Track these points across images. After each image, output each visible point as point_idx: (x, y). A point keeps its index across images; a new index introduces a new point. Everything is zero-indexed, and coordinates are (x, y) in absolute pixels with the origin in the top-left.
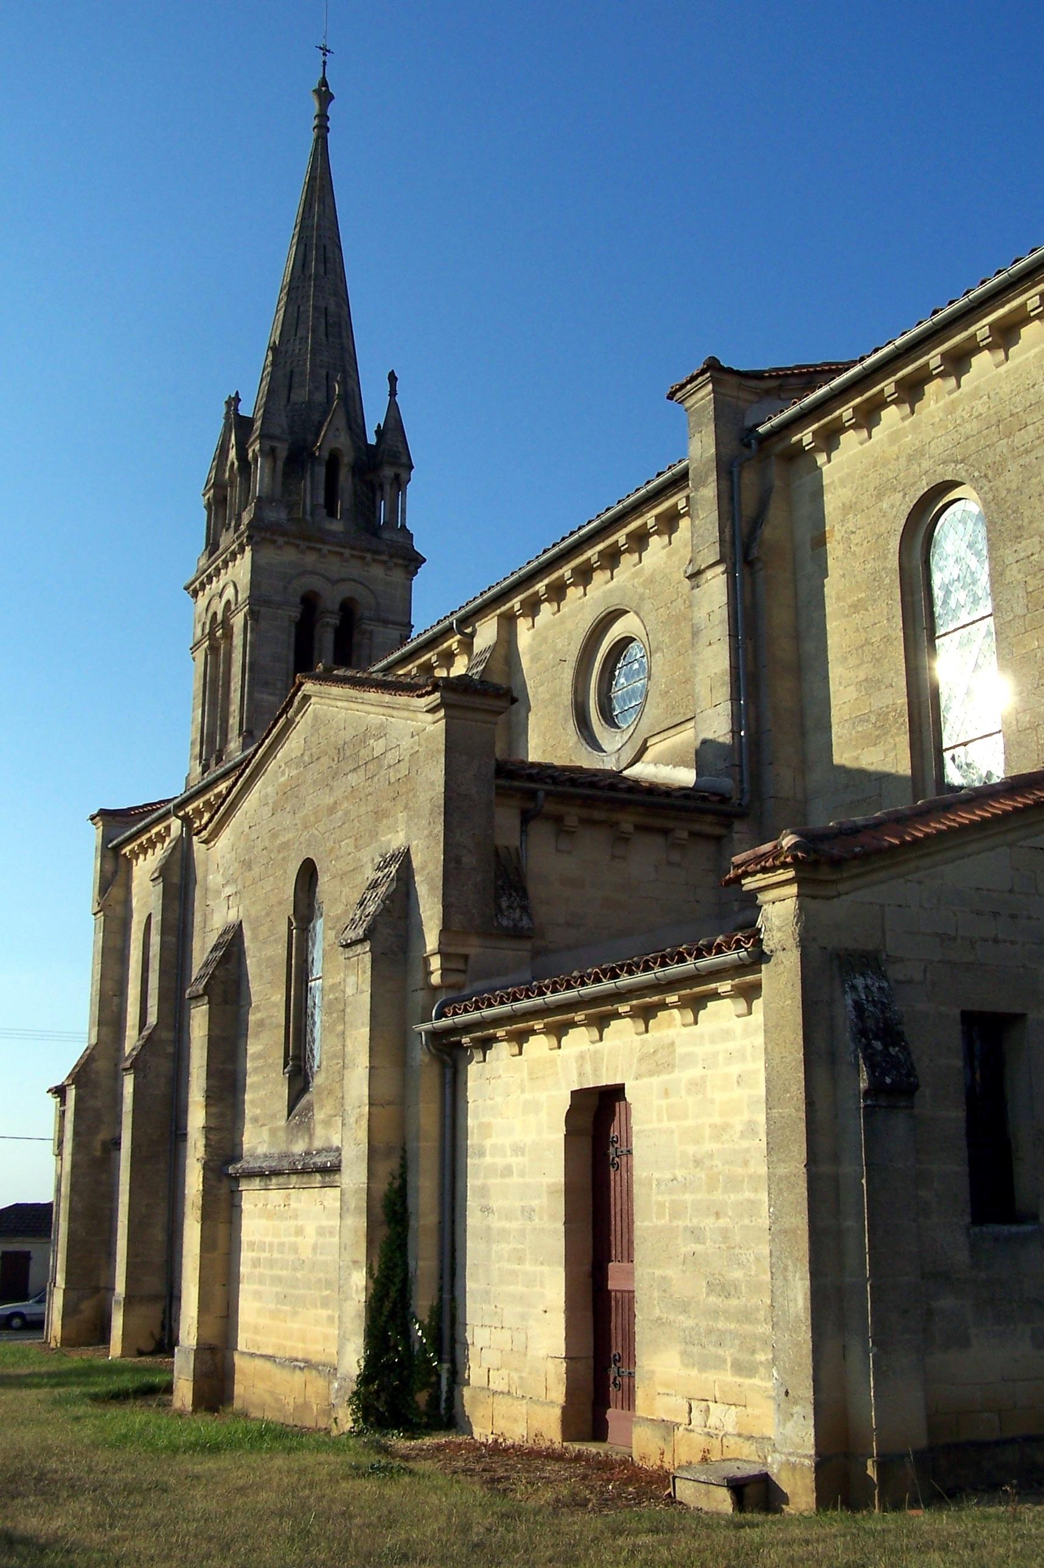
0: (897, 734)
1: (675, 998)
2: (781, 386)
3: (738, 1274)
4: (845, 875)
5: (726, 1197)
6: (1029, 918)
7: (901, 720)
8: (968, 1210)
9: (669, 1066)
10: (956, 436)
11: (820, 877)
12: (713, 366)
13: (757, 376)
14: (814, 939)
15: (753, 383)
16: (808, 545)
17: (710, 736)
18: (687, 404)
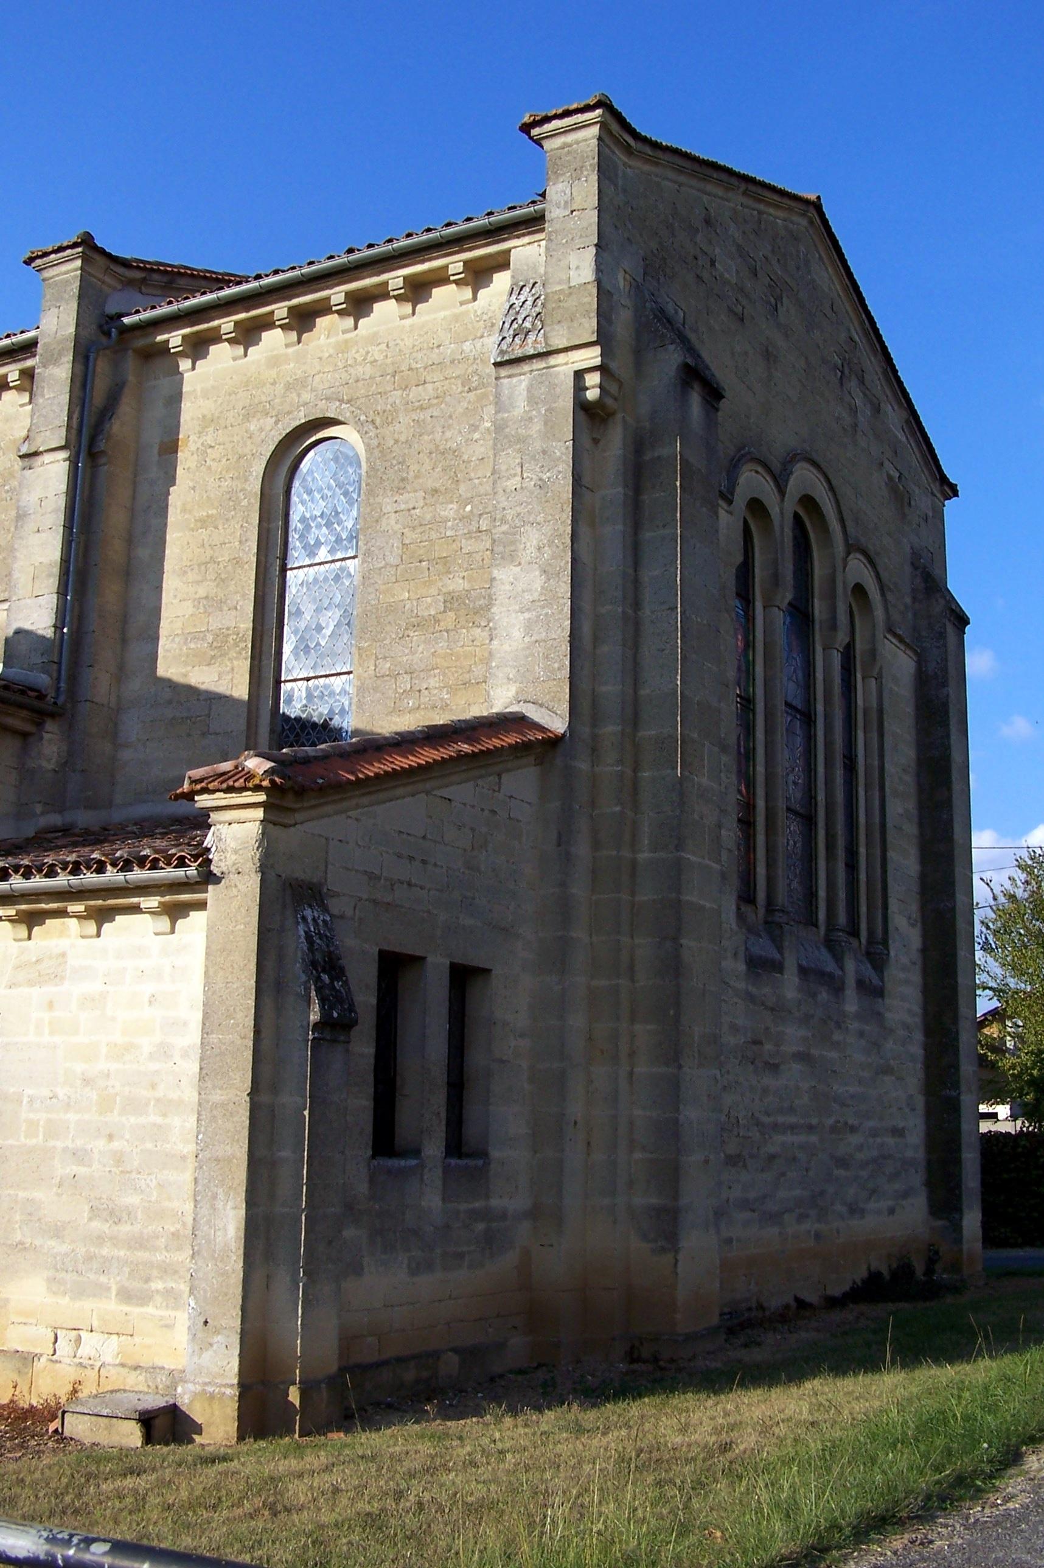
0: (237, 658)
1: (81, 908)
2: (144, 280)
3: (132, 1200)
4: (306, 804)
5: (124, 1119)
6: (435, 865)
7: (243, 645)
8: (371, 1143)
9: (57, 977)
10: (344, 376)
11: (285, 804)
12: (87, 242)
13: (125, 263)
14: (272, 866)
15: (121, 270)
16: (156, 451)
17: (27, 626)
18: (47, 274)
